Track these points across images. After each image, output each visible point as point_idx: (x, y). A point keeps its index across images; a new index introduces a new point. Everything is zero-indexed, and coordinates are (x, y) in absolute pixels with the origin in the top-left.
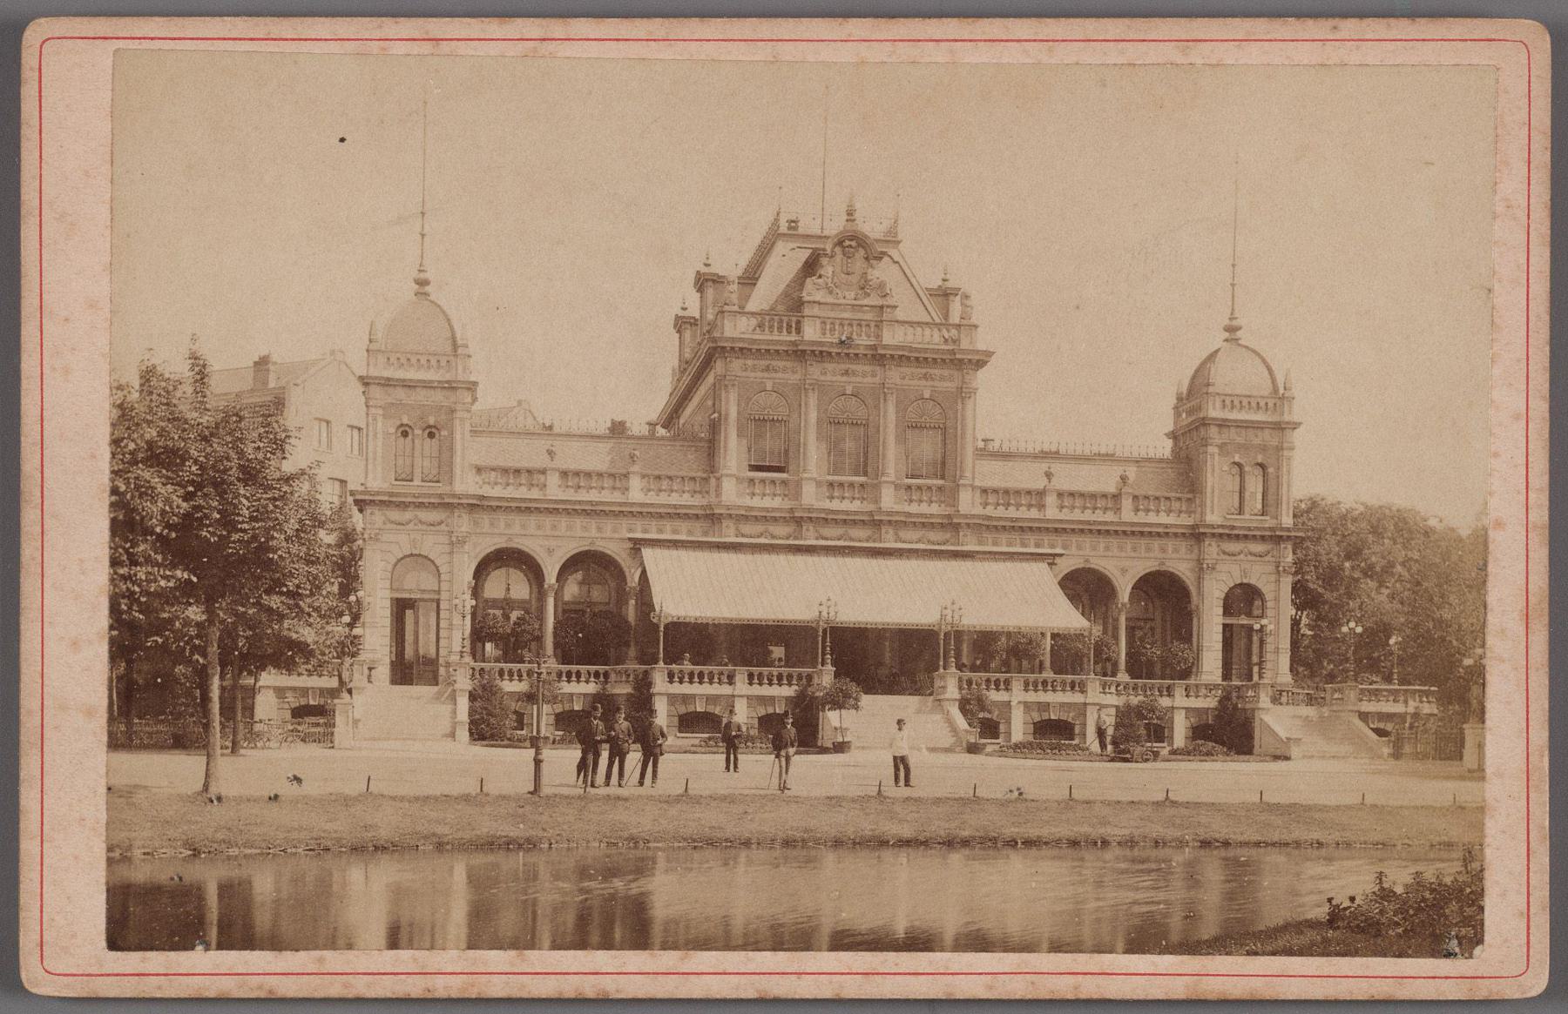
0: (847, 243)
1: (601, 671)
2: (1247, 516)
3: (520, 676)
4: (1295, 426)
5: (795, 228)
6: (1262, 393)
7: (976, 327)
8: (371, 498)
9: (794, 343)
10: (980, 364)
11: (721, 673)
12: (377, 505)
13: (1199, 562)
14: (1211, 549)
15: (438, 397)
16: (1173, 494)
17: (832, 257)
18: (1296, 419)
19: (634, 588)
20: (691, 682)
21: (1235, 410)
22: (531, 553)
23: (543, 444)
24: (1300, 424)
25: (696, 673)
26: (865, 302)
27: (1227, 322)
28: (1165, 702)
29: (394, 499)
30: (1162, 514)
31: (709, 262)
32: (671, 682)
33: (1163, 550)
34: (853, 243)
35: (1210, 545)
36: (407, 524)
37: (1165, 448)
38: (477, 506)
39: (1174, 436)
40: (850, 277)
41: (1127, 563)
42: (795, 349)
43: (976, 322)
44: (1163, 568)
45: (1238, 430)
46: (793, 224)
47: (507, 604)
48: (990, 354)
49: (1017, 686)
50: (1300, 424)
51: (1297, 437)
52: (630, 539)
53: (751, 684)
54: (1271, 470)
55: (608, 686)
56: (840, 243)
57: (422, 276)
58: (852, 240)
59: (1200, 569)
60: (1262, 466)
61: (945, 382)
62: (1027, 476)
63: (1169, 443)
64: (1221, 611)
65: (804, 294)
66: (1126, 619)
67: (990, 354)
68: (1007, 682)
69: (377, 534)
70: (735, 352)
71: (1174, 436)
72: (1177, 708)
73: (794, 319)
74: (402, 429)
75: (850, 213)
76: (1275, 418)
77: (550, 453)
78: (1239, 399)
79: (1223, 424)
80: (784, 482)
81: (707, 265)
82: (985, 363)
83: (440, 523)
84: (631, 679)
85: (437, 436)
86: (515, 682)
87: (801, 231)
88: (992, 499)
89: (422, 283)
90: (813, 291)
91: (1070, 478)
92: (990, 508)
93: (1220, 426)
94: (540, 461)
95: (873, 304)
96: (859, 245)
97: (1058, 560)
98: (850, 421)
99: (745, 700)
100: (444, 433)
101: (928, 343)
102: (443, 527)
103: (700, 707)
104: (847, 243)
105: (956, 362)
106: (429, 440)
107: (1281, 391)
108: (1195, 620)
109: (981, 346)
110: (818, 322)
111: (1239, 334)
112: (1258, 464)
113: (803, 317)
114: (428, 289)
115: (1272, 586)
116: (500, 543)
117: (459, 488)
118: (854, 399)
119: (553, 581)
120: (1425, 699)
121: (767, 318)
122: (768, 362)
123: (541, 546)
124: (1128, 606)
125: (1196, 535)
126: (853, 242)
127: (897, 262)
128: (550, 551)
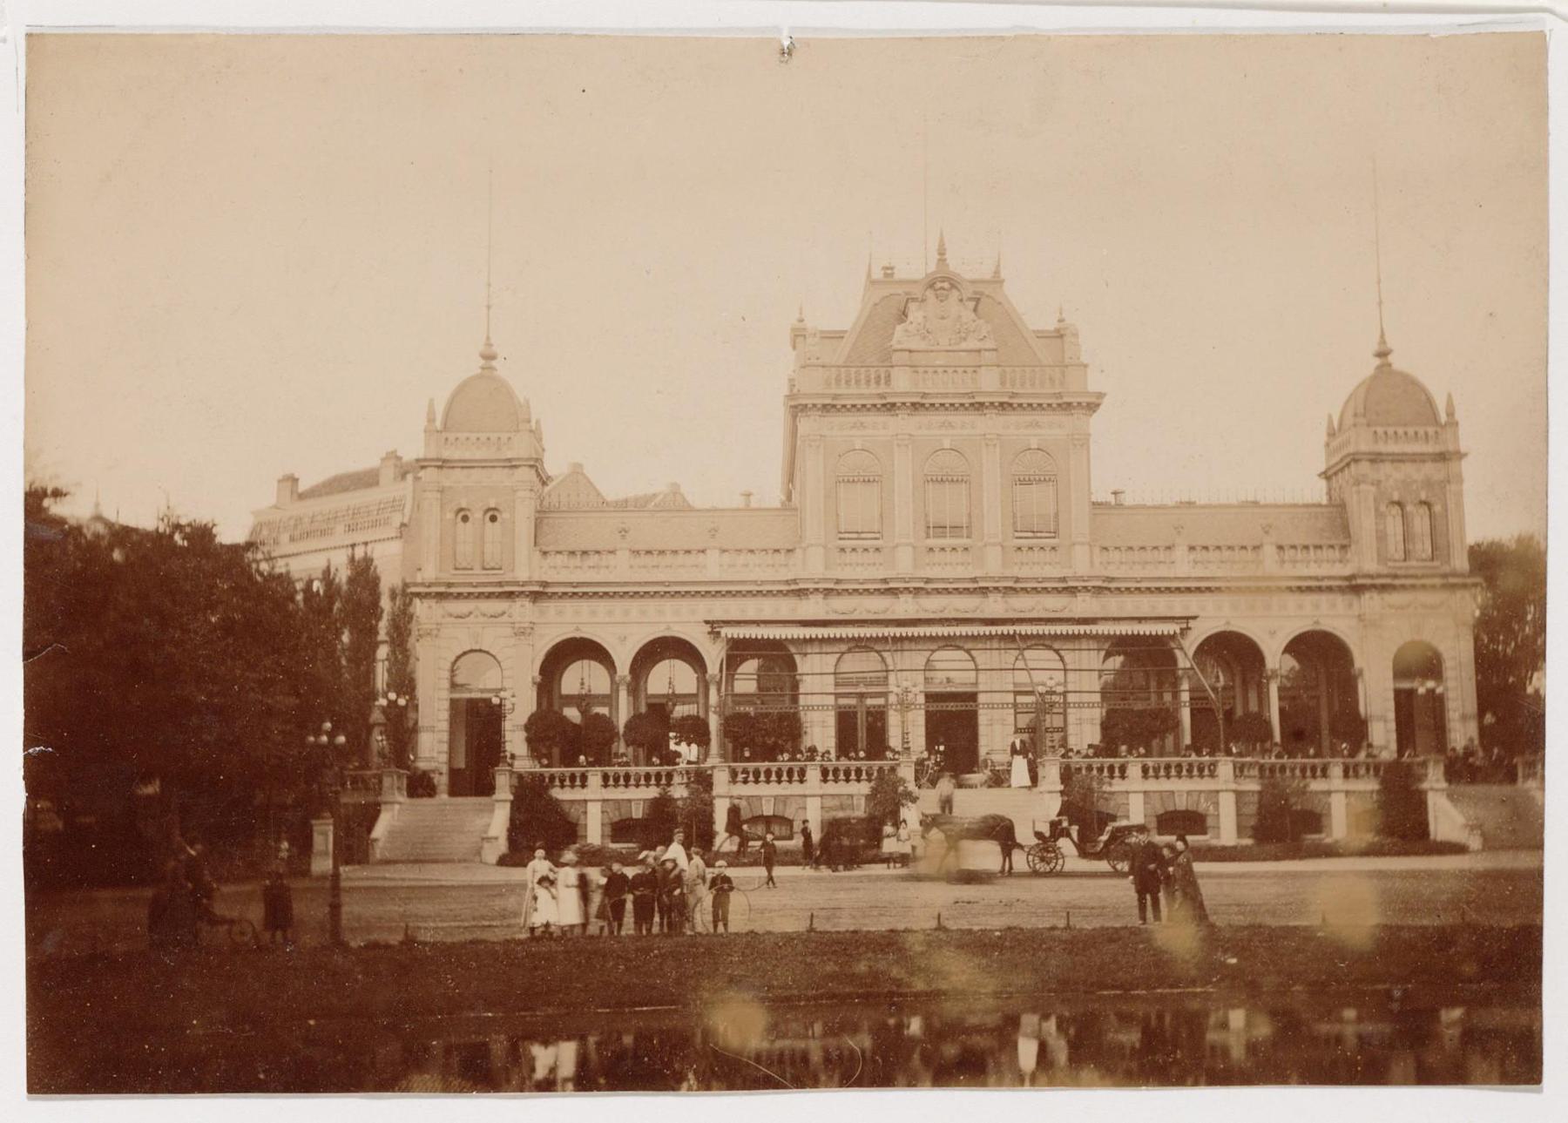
0: (939, 285)
2: (1414, 563)
3: (869, 774)
4: (1460, 455)
5: (892, 275)
7: (1086, 366)
10: (1092, 407)
11: (745, 771)
12: (434, 597)
15: (1429, 469)
16: (1324, 542)
17: (923, 301)
19: (625, 677)
20: (757, 781)
25: (762, 770)
26: (964, 345)
28: (1316, 785)
30: (1312, 564)
32: (606, 785)
33: (1317, 607)
34: (946, 285)
35: (1084, 601)
36: (468, 616)
37: (1317, 492)
39: (1327, 476)
40: (945, 321)
42: (884, 402)
43: (1085, 362)
44: (1318, 628)
45: (1395, 464)
46: (889, 272)
47: (583, 701)
48: (1101, 395)
51: (1467, 467)
53: (825, 780)
54: (1437, 508)
55: (671, 788)
56: (931, 286)
58: (944, 281)
60: (1400, 504)
61: (1053, 428)
66: (1280, 689)
67: (1101, 395)
70: (1083, 408)
74: (462, 514)
76: (1438, 449)
82: (1098, 405)
83: (504, 613)
85: (499, 519)
86: (784, 784)
87: (897, 276)
88: (1289, 554)
89: (489, 357)
92: (1287, 566)
93: (1372, 461)
95: (969, 348)
96: (953, 286)
98: (862, 479)
99: (1141, 795)
100: (506, 515)
102: (505, 618)
103: (1182, 804)
104: (939, 285)
105: (1064, 406)
106: (462, 524)
109: (1093, 387)
111: (1391, 358)
112: (1394, 503)
114: (494, 363)
116: (659, 632)
117: (522, 575)
119: (626, 672)
121: (843, 370)
122: (944, 418)
125: (1354, 587)
128: (1273, 633)
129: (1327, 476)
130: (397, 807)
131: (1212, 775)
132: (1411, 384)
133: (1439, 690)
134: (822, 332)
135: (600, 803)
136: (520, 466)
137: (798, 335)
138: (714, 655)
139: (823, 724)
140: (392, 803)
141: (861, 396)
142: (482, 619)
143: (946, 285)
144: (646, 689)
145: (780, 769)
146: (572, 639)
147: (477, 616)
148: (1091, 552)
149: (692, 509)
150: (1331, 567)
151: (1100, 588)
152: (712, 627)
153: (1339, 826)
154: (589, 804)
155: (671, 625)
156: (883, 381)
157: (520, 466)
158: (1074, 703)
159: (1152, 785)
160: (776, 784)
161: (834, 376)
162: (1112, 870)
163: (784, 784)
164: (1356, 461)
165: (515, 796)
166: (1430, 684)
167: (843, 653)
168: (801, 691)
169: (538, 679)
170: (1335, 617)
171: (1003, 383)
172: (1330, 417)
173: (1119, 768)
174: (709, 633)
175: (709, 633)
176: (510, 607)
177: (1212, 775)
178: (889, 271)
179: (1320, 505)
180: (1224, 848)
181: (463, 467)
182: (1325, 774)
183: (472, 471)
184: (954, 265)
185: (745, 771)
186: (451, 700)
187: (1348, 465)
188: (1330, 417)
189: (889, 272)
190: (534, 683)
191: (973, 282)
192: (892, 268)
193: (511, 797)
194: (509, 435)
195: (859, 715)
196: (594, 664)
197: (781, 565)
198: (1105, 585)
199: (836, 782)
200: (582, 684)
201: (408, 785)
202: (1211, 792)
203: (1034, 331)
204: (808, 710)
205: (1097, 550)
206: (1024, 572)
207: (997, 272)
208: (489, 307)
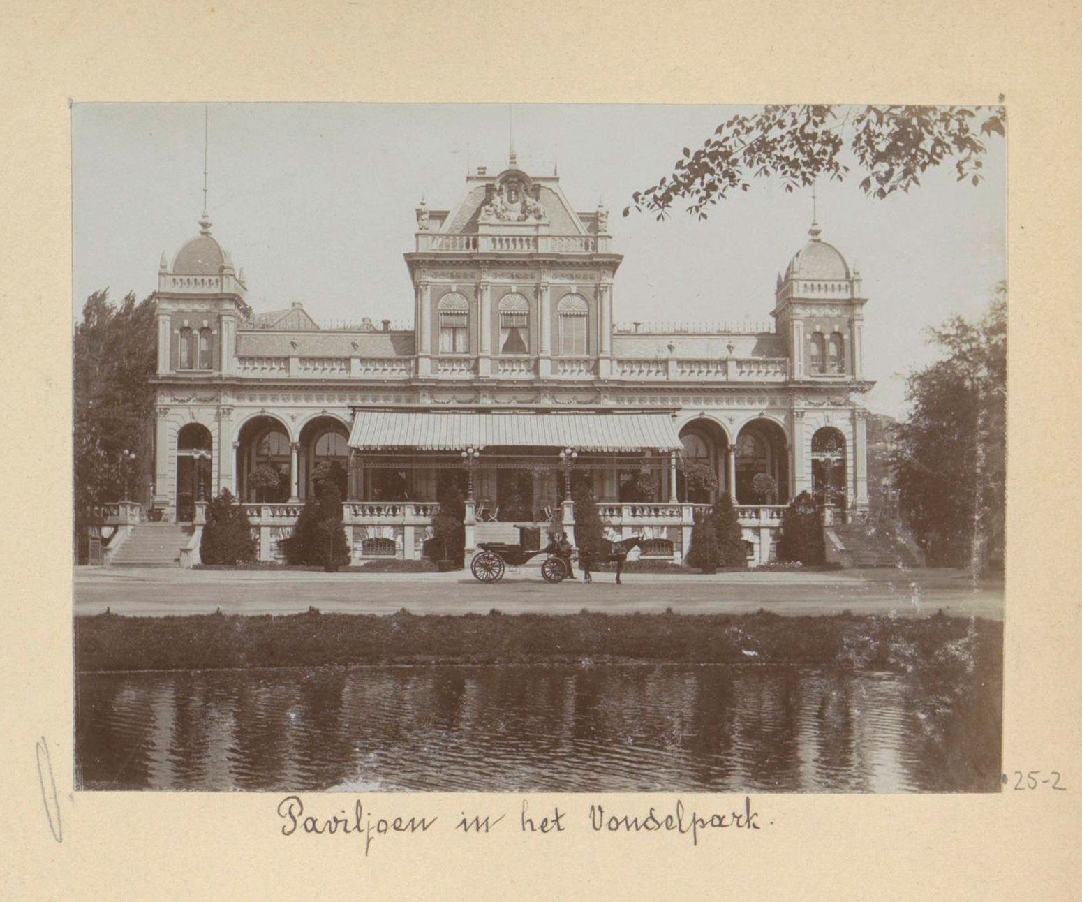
1: (375, 507)
4: (862, 302)
5: (484, 173)
6: (837, 277)
8: (483, 385)
9: (470, 255)
13: (791, 411)
14: (800, 404)
18: (864, 296)
21: (828, 292)
22: (752, 419)
23: (725, 341)
24: (866, 300)
27: (810, 227)
29: (177, 382)
31: (424, 202)
38: (239, 387)
39: (775, 314)
41: (731, 414)
42: (470, 259)
46: (482, 171)
49: (626, 512)
50: (866, 300)
52: (349, 407)
54: (846, 337)
57: (815, 228)
59: (791, 416)
62: (648, 349)
63: (773, 320)
64: (810, 449)
65: (480, 219)
66: (736, 458)
68: (619, 509)
69: (228, 409)
71: (775, 314)
72: (762, 528)
73: (471, 238)
75: (513, 158)
77: (729, 347)
78: (818, 283)
79: (806, 303)
80: (527, 361)
81: (423, 204)
84: (781, 515)
87: (487, 174)
89: (205, 225)
90: (486, 217)
91: (687, 349)
94: (722, 353)
97: (677, 413)
101: (567, 251)
104: (511, 179)
107: (852, 275)
108: (790, 457)
109: (614, 250)
110: (490, 238)
111: (210, 230)
113: (478, 236)
115: (850, 428)
118: (459, 295)
120: (278, 514)
123: (287, 415)
124: (299, 445)
125: (788, 390)
126: (515, 181)
127: (556, 193)
130: (130, 528)
133: (209, 456)
134: (431, 212)
135: (269, 529)
137: (419, 213)
139: (802, 480)
140: (126, 525)
143: (516, 180)
144: (315, 450)
148: (612, 364)
149: (317, 330)
150: (772, 375)
151: (616, 388)
153: (267, 547)
154: (406, 528)
155: (265, 409)
156: (471, 246)
161: (465, 242)
162: (591, 573)
165: (577, 521)
166: (203, 452)
169: (238, 444)
172: (779, 277)
177: (758, 517)
178: (482, 170)
180: (409, 562)
182: (620, 514)
184: (523, 166)
186: (180, 458)
188: (779, 277)
189: (482, 171)
190: (234, 447)
191: (534, 179)
192: (485, 168)
193: (574, 522)
195: (440, 467)
196: (332, 435)
198: (620, 386)
199: (273, 516)
200: (329, 448)
202: (675, 526)
203: (578, 214)
205: (615, 363)
206: (441, 376)
207: (555, 174)
208: (205, 191)
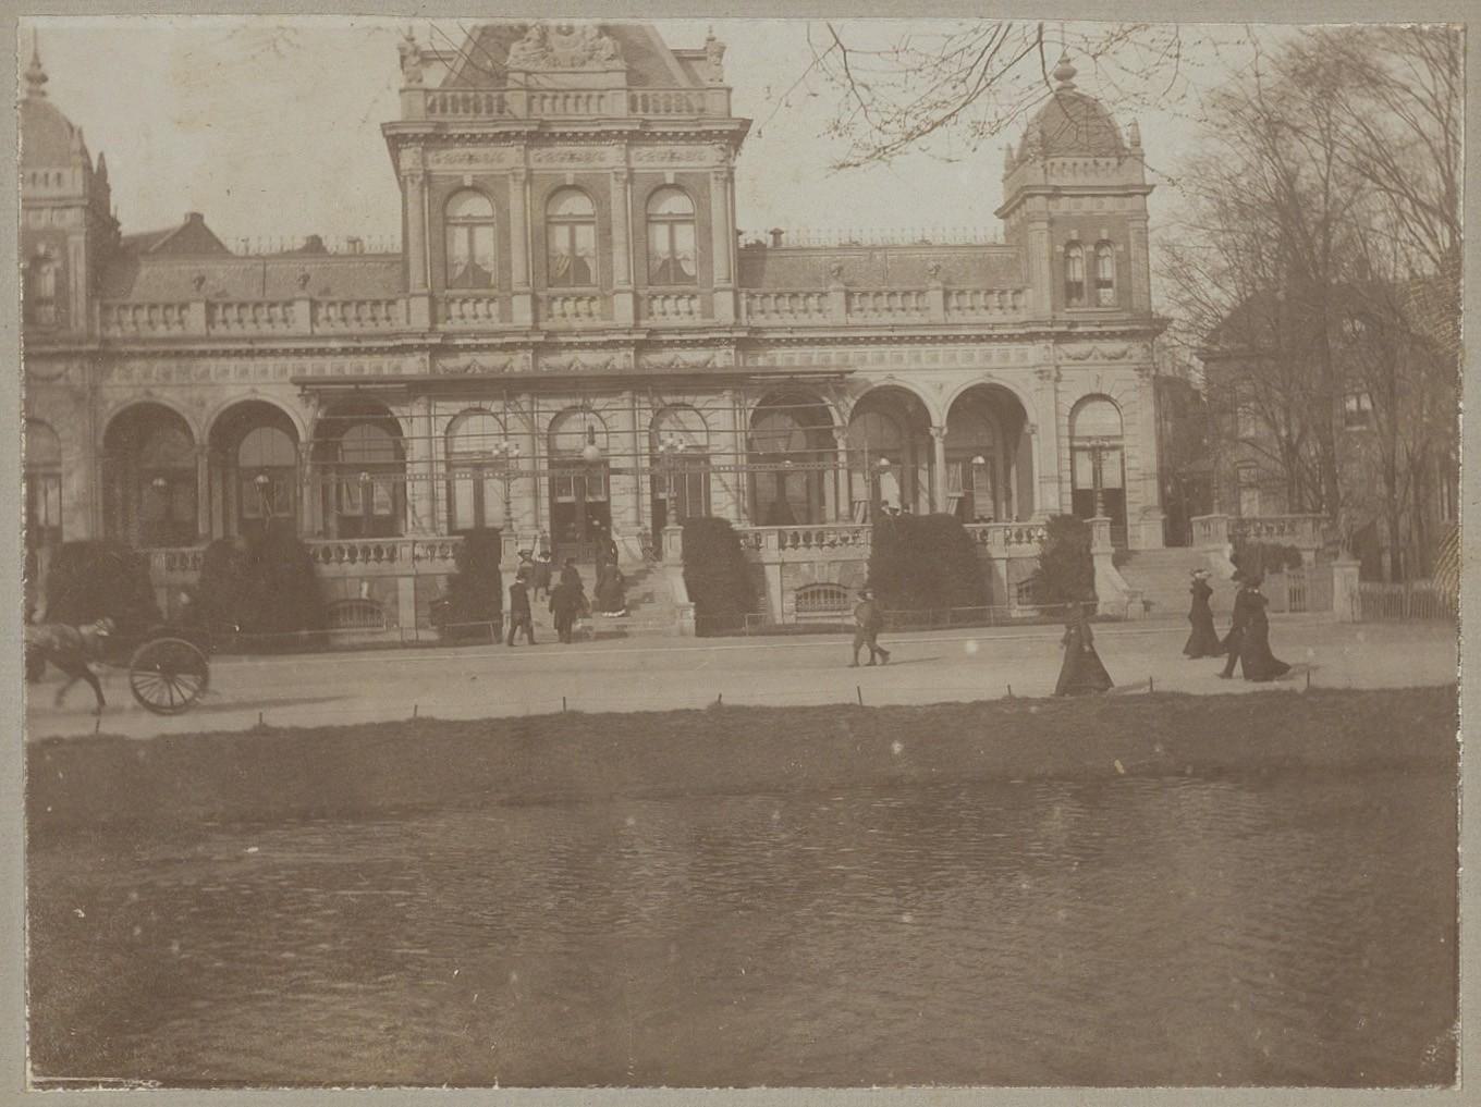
7: (729, 90)
39: (1003, 214)
48: (747, 123)
67: (747, 123)
102: (61, 381)
109: (739, 112)
114: (44, 87)
129: (1003, 214)
131: (1293, 532)
132: (1091, 107)
136: (1036, 195)
138: (304, 417)
141: (675, 123)
142: (1101, 360)
145: (796, 533)
146: (274, 406)
147: (1096, 358)
152: (303, 389)
157: (1036, 195)
158: (421, 480)
159: (790, 555)
160: (803, 549)
163: (813, 549)
164: (1032, 196)
167: (455, 417)
168: (408, 459)
170: (1014, 368)
171: (633, 109)
173: (817, 535)
174: (299, 396)
175: (299, 396)
176: (511, 360)
179: (995, 245)
181: (1072, 196)
183: (1104, 200)
185: (184, 556)
187: (1023, 201)
194: (1107, 160)
196: (278, 433)
197: (800, 311)
201: (686, 555)
204: (415, 480)
